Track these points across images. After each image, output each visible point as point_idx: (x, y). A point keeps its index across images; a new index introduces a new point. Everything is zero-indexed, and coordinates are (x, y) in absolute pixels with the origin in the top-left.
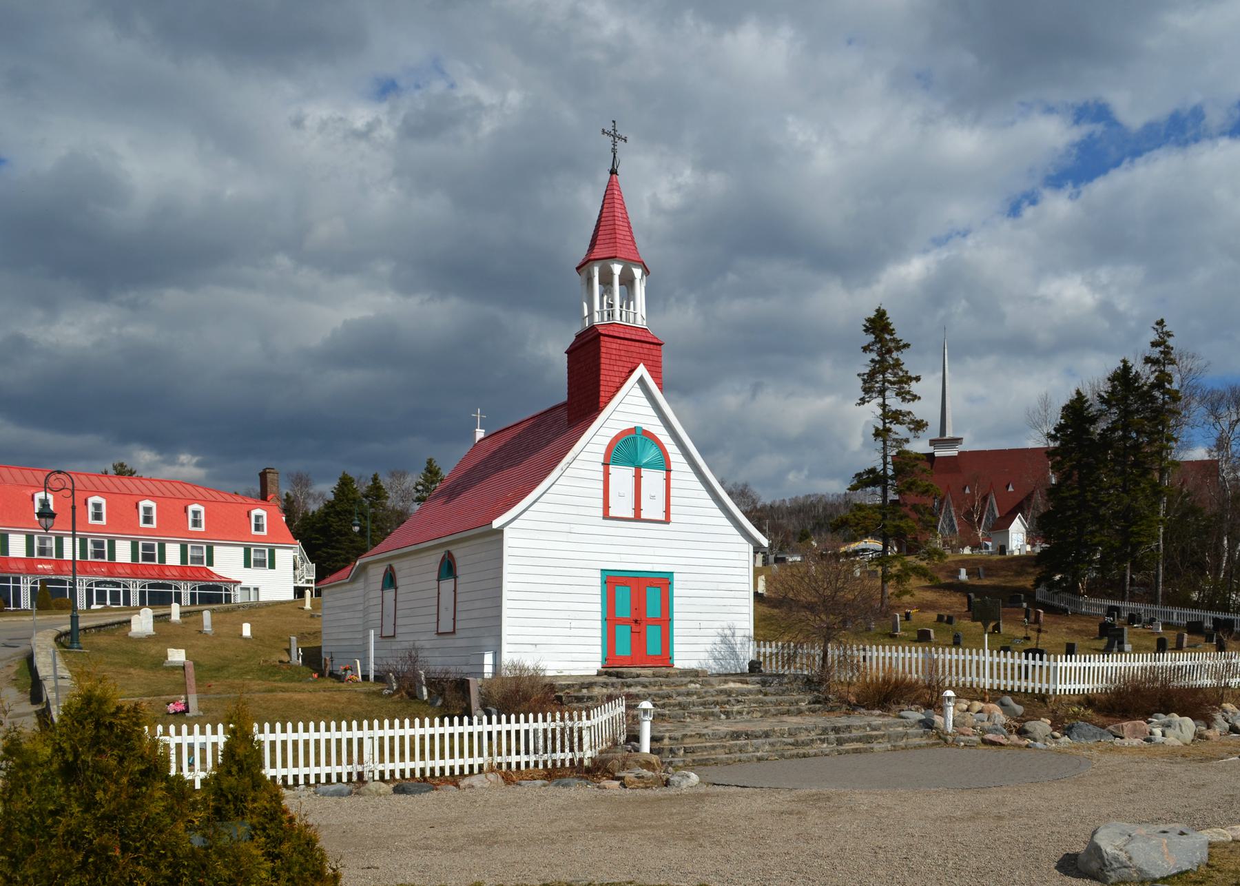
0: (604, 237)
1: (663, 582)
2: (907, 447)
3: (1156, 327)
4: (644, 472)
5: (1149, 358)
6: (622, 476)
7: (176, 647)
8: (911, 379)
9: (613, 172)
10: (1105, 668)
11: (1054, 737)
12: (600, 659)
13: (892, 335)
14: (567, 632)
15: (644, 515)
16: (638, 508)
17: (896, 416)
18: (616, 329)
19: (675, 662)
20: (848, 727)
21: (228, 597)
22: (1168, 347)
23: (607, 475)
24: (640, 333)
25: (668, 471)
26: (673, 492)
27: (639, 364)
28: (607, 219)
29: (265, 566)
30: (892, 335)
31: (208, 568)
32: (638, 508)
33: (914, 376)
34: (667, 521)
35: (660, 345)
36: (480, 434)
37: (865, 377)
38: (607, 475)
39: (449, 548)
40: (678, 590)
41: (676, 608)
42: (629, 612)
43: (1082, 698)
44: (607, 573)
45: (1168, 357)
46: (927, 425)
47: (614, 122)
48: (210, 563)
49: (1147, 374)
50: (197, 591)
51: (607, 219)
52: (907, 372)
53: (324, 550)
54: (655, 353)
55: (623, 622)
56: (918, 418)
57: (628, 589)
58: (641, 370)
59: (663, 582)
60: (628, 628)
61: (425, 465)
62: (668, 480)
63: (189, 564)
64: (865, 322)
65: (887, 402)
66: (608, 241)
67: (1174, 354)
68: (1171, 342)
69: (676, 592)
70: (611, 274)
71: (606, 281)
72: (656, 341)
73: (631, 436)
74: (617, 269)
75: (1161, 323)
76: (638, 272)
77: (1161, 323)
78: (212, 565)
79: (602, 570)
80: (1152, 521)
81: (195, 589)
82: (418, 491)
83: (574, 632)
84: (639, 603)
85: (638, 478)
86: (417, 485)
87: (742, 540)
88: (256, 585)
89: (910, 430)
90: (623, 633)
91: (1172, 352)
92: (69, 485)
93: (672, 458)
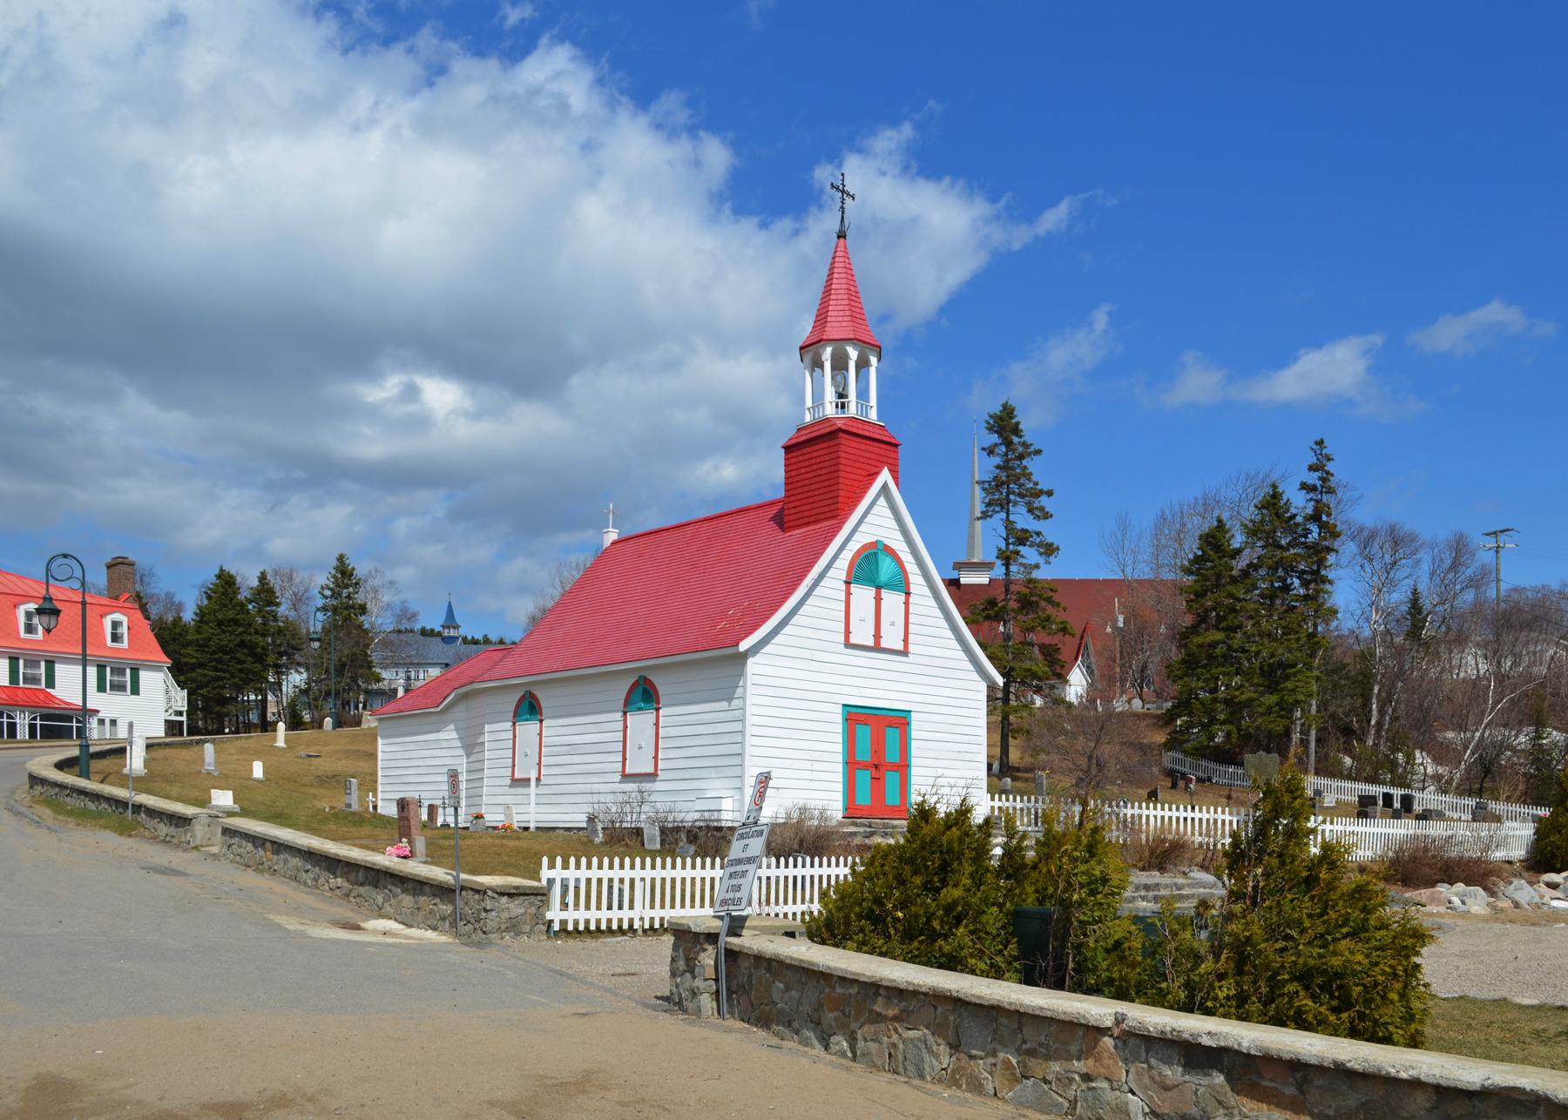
0: (836, 313)
1: (900, 721)
2: (1036, 575)
3: (1314, 447)
4: (884, 593)
5: (1305, 483)
6: (863, 596)
7: (222, 788)
8: (1040, 493)
13: (1020, 437)
14: (808, 775)
15: (884, 644)
16: (877, 636)
17: (1023, 538)
18: (866, 428)
20: (1157, 885)
21: (81, 733)
22: (1328, 473)
23: (848, 594)
24: (877, 431)
25: (908, 594)
26: (912, 619)
28: (838, 292)
29: (125, 691)
30: (1020, 437)
31: (48, 690)
32: (877, 636)
33: (1045, 489)
34: (904, 653)
35: (896, 445)
36: (612, 535)
37: (986, 486)
38: (848, 594)
40: (916, 731)
41: (913, 753)
42: (869, 754)
43: (1355, 864)
44: (848, 709)
45: (1327, 484)
46: (1058, 549)
48: (51, 682)
49: (1299, 503)
50: (38, 722)
51: (838, 292)
52: (1036, 484)
53: (199, 670)
54: (892, 455)
55: (864, 766)
56: (1049, 540)
57: (868, 729)
58: (885, 476)
59: (900, 721)
60: (868, 773)
61: (335, 563)
62: (907, 603)
63: (21, 685)
64: (987, 418)
65: (1012, 518)
66: (841, 319)
67: (1333, 482)
68: (1330, 467)
69: (914, 734)
70: (846, 357)
71: (840, 364)
72: (893, 441)
73: (872, 551)
74: (853, 353)
75: (1320, 443)
76: (873, 360)
77: (1320, 443)
78: (53, 687)
80: (1308, 677)
81: (34, 719)
82: (326, 597)
84: (878, 746)
85: (878, 599)
86: (322, 588)
87: (976, 676)
88: (113, 716)
89: (1041, 554)
90: (864, 777)
91: (1331, 478)
92: (78, 573)
93: (912, 578)
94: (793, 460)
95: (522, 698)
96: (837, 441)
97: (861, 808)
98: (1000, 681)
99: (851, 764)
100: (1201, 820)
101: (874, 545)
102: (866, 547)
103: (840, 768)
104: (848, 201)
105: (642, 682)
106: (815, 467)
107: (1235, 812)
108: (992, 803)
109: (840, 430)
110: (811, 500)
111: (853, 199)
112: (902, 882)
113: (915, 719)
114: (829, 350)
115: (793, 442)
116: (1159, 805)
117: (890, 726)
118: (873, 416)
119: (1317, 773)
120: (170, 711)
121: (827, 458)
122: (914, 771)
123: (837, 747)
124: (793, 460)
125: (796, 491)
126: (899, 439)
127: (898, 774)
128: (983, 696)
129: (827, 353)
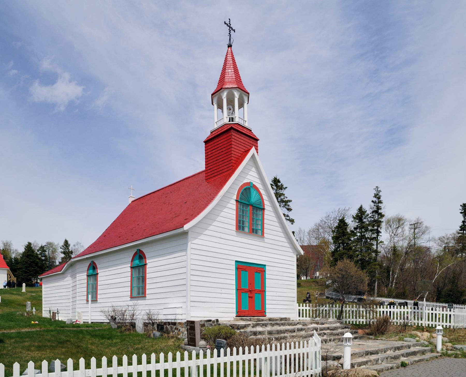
9: (230, 46)
10: (445, 321)
11: (102, 344)
12: (235, 312)
19: (267, 314)
27: (251, 147)
39: (93, 260)
41: (267, 285)
47: (229, 19)
55: (246, 291)
69: (267, 276)
70: (233, 96)
79: (236, 261)
83: (223, 296)
84: (251, 282)
90: (245, 296)
94: (209, 147)
95: (90, 264)
96: (230, 134)
97: (244, 312)
99: (239, 290)
101: (248, 184)
102: (245, 184)
103: (234, 292)
104: (232, 32)
105: (138, 252)
106: (220, 148)
107: (308, 306)
108: (299, 308)
109: (232, 128)
110: (218, 164)
115: (210, 137)
117: (257, 272)
119: (378, 297)
121: (225, 143)
122: (267, 293)
123: (233, 281)
124: (209, 147)
125: (210, 162)
126: (258, 137)
127: (260, 295)
129: (224, 95)
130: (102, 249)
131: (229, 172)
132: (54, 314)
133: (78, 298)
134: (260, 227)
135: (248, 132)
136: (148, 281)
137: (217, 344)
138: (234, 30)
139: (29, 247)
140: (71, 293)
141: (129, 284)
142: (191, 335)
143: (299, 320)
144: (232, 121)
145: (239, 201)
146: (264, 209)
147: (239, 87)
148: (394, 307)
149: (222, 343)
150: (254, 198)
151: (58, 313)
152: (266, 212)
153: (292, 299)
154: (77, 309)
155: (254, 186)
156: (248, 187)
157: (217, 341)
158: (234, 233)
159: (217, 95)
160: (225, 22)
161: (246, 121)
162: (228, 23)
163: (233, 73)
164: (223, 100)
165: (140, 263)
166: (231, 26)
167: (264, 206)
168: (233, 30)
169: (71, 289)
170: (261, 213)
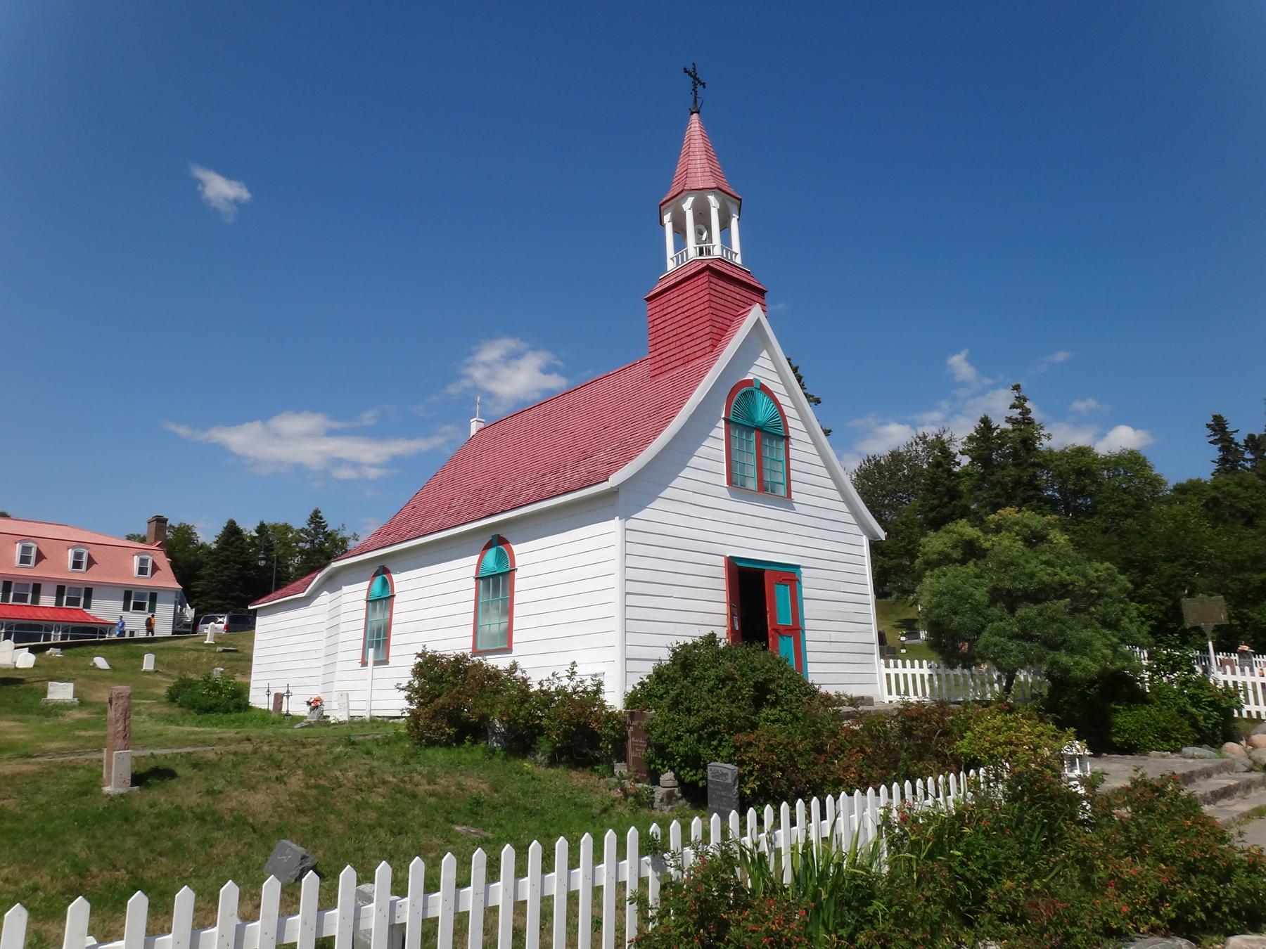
36: (474, 427)
59: (790, 575)
69: (805, 592)
78: (89, 608)
98: (882, 535)
100: (905, 676)
104: (700, 87)
111: (704, 87)
112: (807, 783)
113: (806, 577)
114: (690, 200)
116: (899, 662)
117: (780, 583)
118: (738, 260)
120: (181, 625)
128: (866, 550)
130: (451, 521)
131: (705, 359)
132: (279, 698)
133: (340, 656)
134: (781, 478)
135: (743, 274)
136: (517, 611)
137: (713, 777)
138: (704, 85)
139: (232, 531)
140: (325, 643)
141: (470, 618)
142: (637, 749)
143: (890, 702)
144: (709, 254)
145: (732, 419)
146: (787, 438)
147: (720, 186)
148: (1252, 670)
149: (727, 774)
150: (763, 412)
151: (288, 697)
152: (794, 445)
153: (867, 648)
154: (336, 684)
155: (763, 388)
156: (750, 388)
157: (713, 768)
158: (725, 492)
159: (672, 205)
160: (685, 69)
161: (736, 254)
162: (691, 70)
163: (706, 161)
164: (684, 214)
165: (499, 568)
166: (697, 76)
167: (787, 431)
168: (701, 84)
169: (325, 635)
170: (782, 445)
